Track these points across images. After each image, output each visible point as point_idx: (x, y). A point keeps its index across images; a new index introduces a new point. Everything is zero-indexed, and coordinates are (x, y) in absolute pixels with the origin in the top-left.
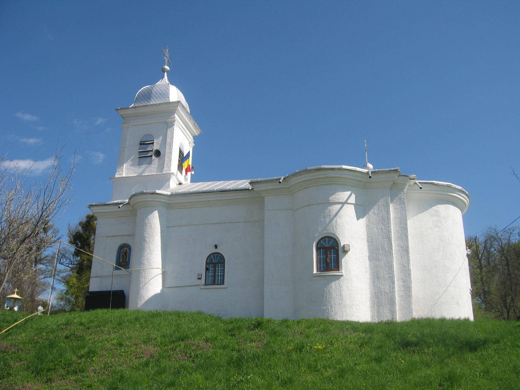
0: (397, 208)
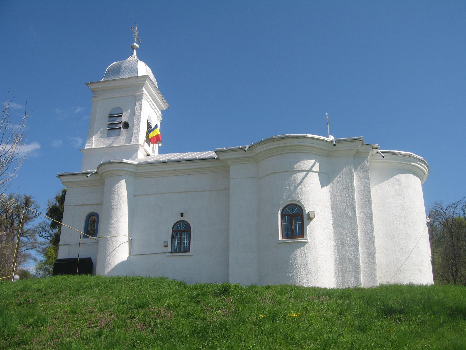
0: (360, 176)
